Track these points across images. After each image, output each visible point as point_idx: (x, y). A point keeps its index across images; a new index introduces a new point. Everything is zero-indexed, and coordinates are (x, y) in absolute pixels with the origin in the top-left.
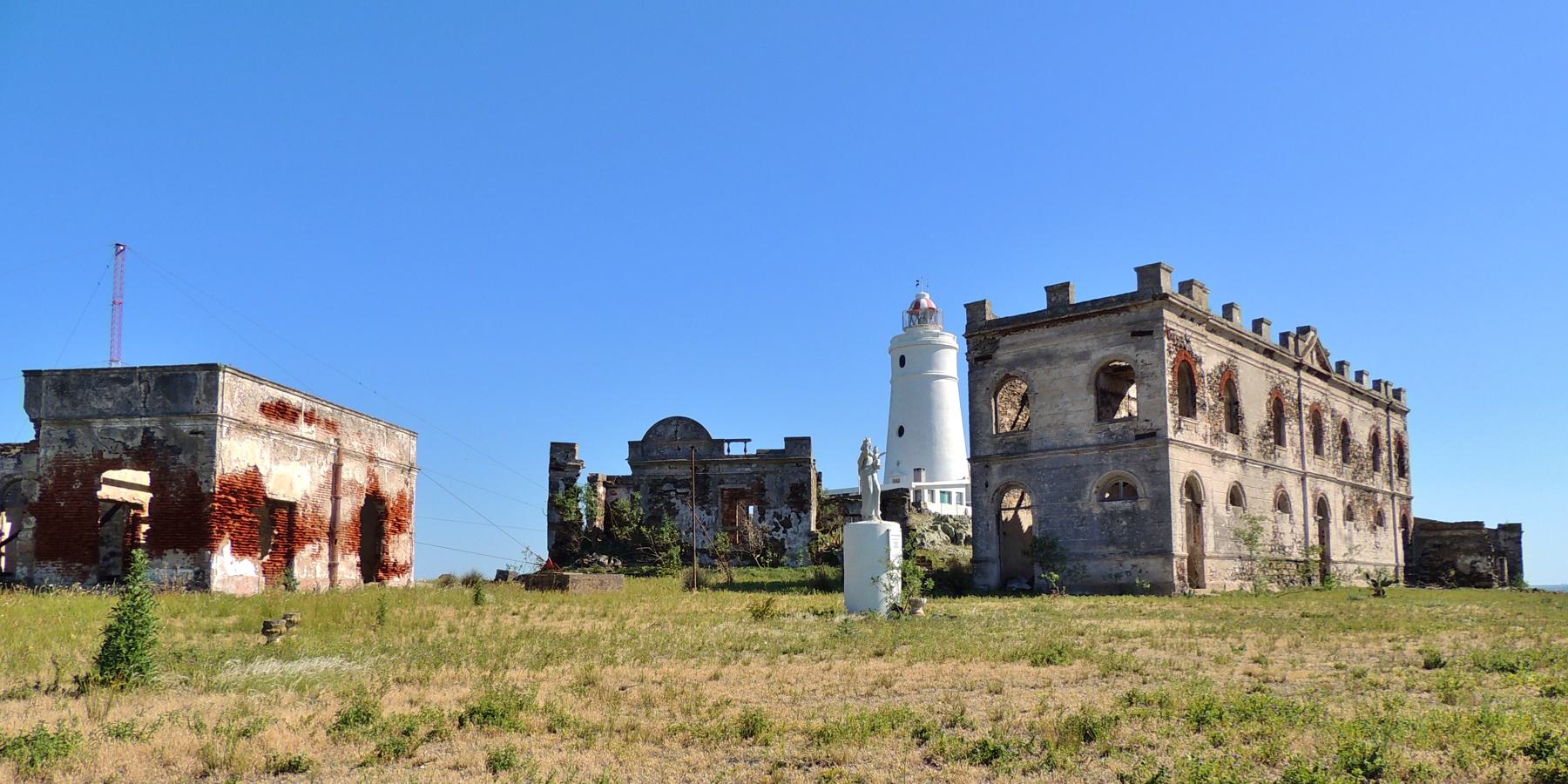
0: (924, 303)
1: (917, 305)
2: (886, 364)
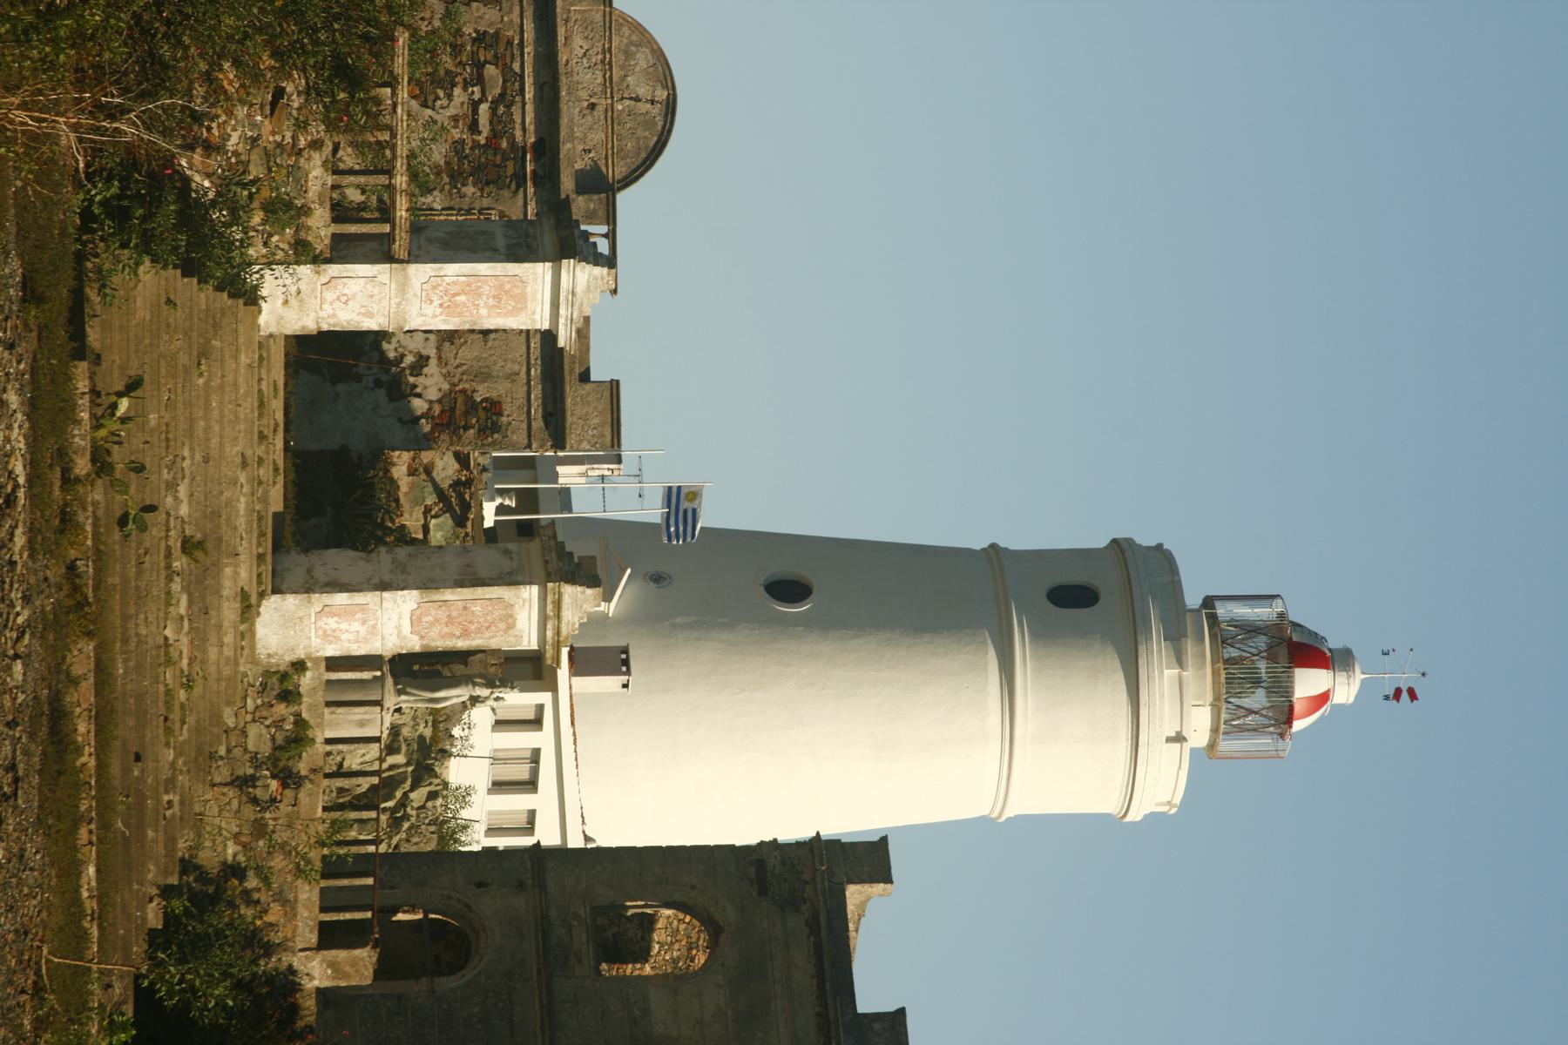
0: (1308, 682)
1: (1310, 653)
2: (1067, 523)
